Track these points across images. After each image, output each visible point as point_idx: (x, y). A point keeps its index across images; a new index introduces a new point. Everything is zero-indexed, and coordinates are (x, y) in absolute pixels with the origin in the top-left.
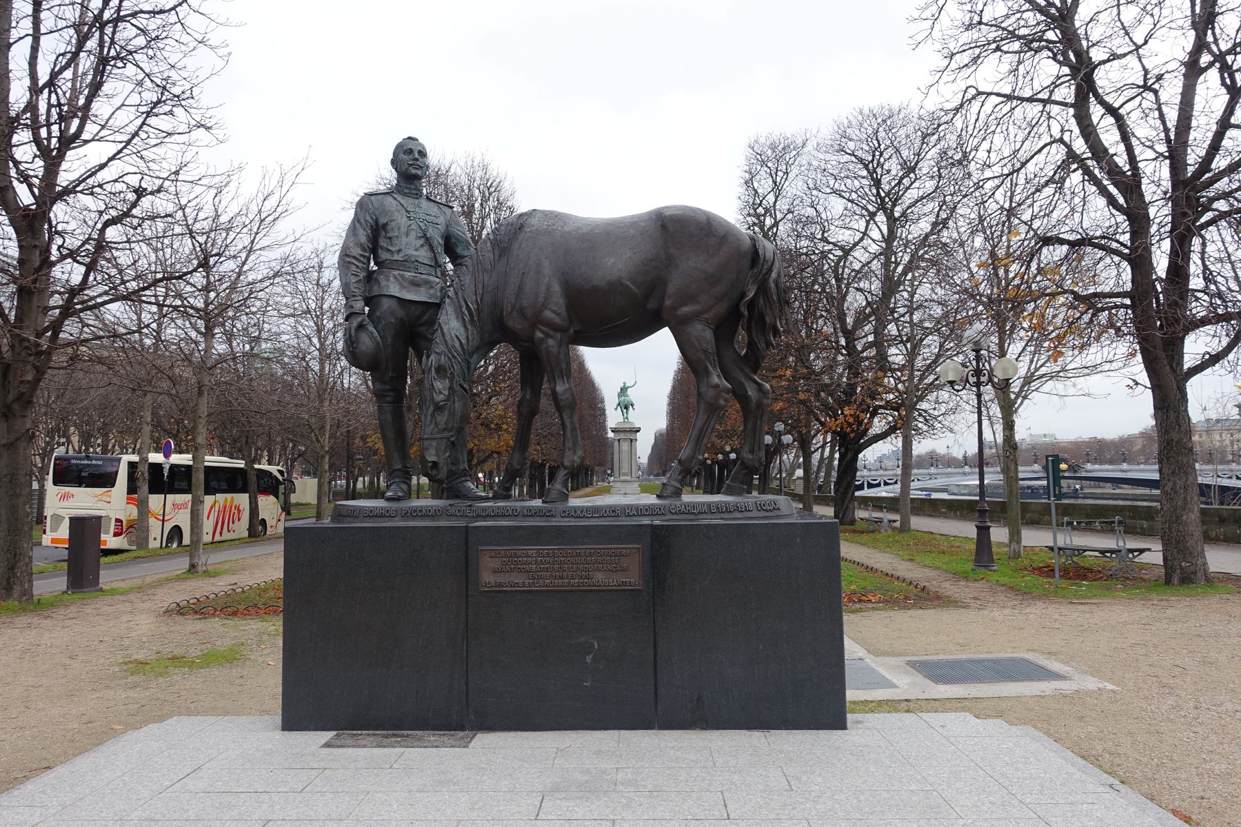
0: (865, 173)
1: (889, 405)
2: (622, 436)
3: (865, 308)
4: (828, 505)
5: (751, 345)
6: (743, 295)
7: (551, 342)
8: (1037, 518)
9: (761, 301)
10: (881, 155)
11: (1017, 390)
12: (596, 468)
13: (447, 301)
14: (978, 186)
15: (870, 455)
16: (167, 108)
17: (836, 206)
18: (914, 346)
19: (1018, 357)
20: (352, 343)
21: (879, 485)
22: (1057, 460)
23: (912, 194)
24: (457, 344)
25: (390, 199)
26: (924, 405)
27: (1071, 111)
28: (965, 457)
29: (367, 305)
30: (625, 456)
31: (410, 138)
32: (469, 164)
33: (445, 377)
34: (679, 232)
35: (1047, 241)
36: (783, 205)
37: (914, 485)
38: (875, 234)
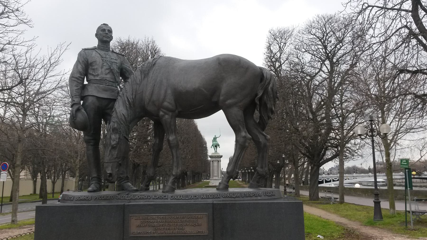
0: (320, 43)
1: (332, 146)
2: (214, 159)
3: (321, 102)
4: (307, 190)
5: (261, 117)
6: (256, 95)
7: (167, 116)
8: (403, 197)
9: (265, 97)
10: (327, 35)
11: (391, 138)
12: (203, 174)
13: (119, 98)
14: (370, 47)
15: (326, 167)
16: (6, 16)
17: (307, 57)
18: (344, 118)
19: (391, 124)
20: (74, 118)
21: (330, 181)
22: (410, 171)
23: (341, 52)
24: (123, 118)
25: (94, 53)
26: (349, 145)
27: (410, 14)
28: (369, 169)
29: (82, 100)
30: (215, 168)
31: (104, 24)
32: (147, 40)
33: (117, 133)
34: (230, 65)
35: (402, 71)
36: (284, 57)
37: (345, 182)
38: (324, 68)
